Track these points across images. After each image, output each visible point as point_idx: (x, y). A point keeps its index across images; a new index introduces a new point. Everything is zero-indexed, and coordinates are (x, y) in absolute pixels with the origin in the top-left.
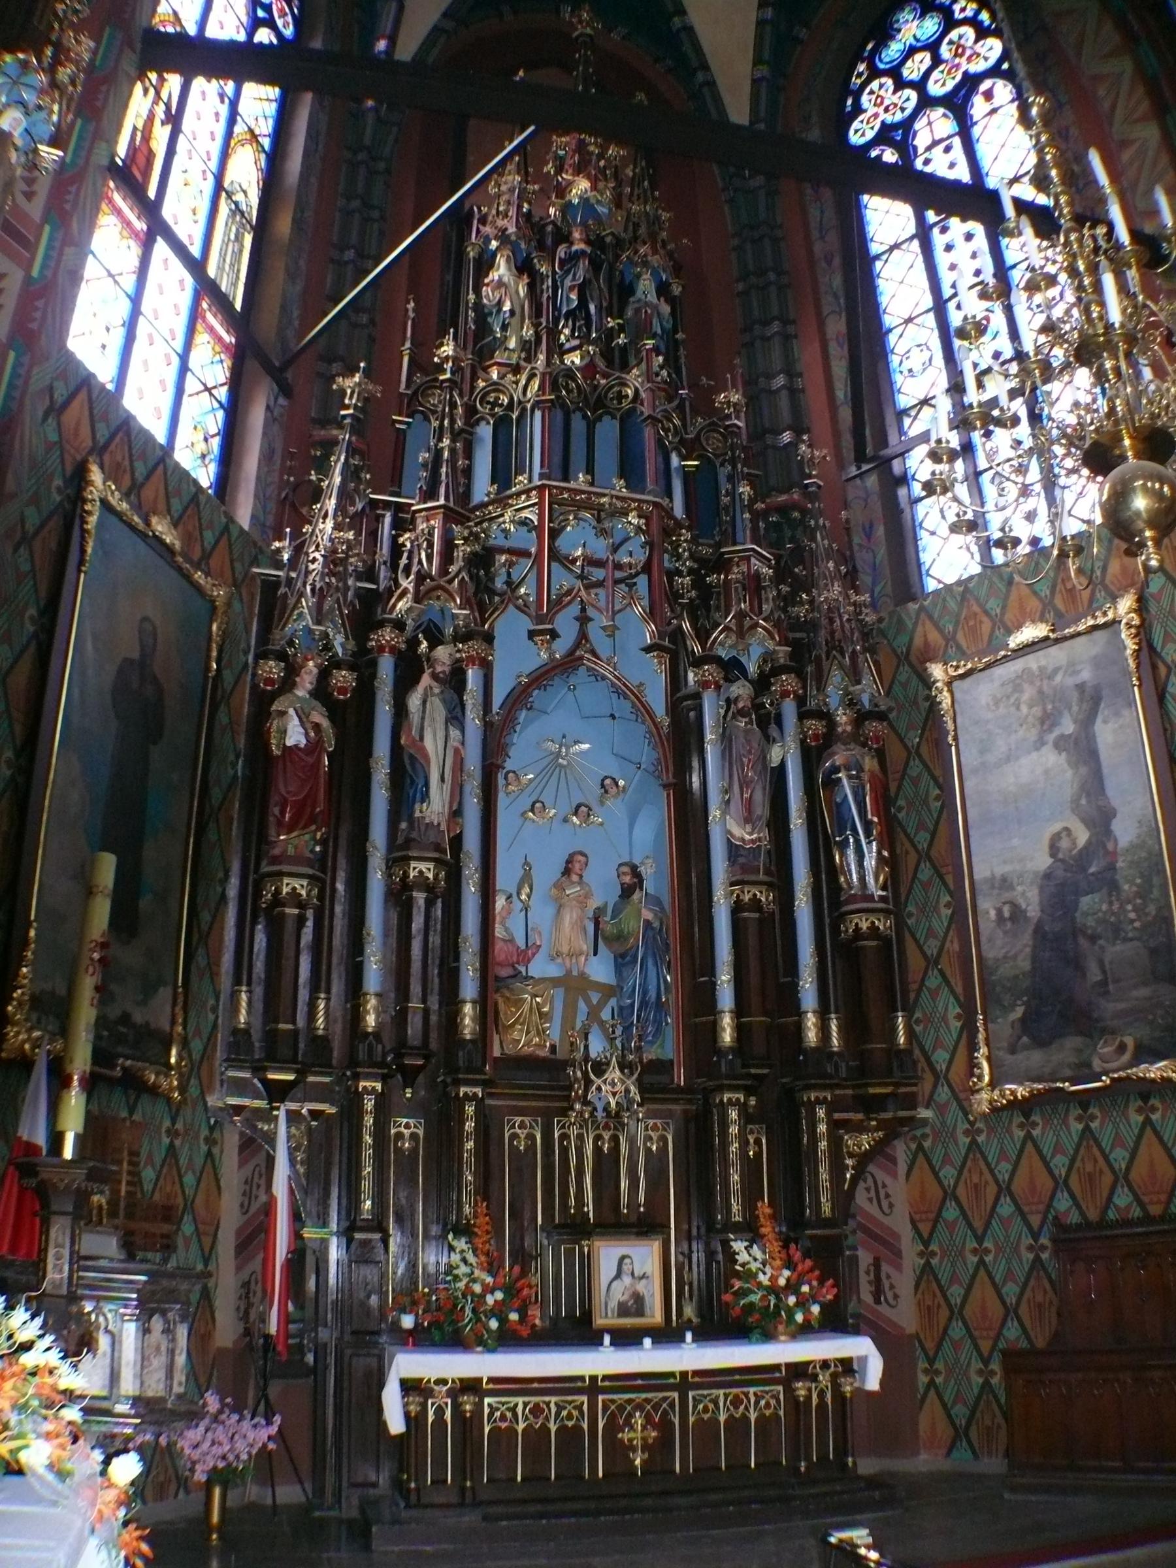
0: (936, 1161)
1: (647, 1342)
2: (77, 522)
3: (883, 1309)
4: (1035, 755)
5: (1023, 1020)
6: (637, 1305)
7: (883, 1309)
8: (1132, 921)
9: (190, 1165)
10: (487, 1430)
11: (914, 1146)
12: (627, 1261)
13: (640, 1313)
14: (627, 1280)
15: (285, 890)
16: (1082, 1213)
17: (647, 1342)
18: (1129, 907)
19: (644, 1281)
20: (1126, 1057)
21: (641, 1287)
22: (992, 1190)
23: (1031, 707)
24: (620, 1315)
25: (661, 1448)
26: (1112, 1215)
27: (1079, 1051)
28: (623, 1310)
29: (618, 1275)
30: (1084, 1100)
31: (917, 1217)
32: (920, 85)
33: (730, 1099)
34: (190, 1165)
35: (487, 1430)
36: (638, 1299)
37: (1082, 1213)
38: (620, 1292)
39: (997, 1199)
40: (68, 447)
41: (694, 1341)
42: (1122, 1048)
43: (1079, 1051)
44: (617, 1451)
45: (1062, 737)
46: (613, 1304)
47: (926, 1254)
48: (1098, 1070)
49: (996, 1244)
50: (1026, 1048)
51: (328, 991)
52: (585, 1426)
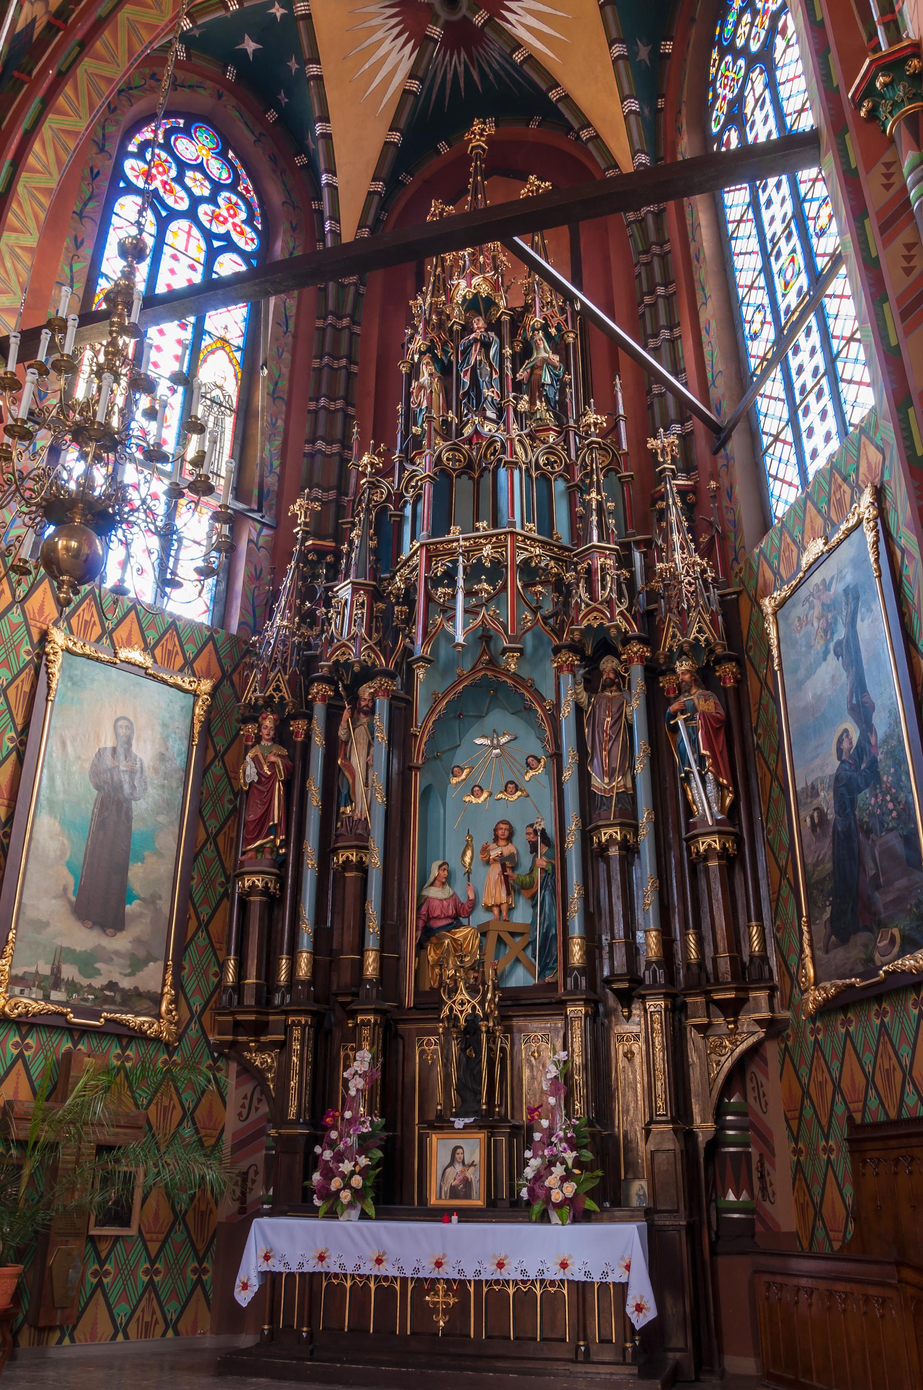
0: (796, 1059)
1: (455, 1218)
2: (43, 669)
3: (767, 1204)
4: (824, 664)
5: (832, 920)
6: (463, 1189)
7: (767, 1204)
8: (891, 811)
9: (866, 1043)
10: (324, 1284)
11: (783, 1046)
12: (459, 1151)
13: (468, 1196)
14: (458, 1167)
15: (702, 849)
16: (886, 1114)
17: (455, 1218)
18: (888, 798)
19: (472, 1169)
20: (896, 949)
21: (471, 1174)
22: (178, 1114)
23: (819, 620)
24: (451, 1198)
25: (458, 1313)
26: (905, 1114)
27: (866, 946)
28: (454, 1193)
29: (452, 1164)
30: (85, 1031)
31: (789, 1115)
32: (217, 187)
33: (293, 1021)
34: (866, 1043)
35: (324, 1284)
36: (467, 1182)
37: (886, 1114)
38: (454, 1175)
39: (180, 1124)
40: (32, 622)
41: (459, 1221)
42: (893, 941)
43: (866, 946)
44: (423, 1312)
45: (839, 644)
46: (446, 1188)
47: (797, 1152)
48: (879, 964)
49: (836, 1143)
50: (836, 946)
51: (759, 918)
52: (398, 1288)
